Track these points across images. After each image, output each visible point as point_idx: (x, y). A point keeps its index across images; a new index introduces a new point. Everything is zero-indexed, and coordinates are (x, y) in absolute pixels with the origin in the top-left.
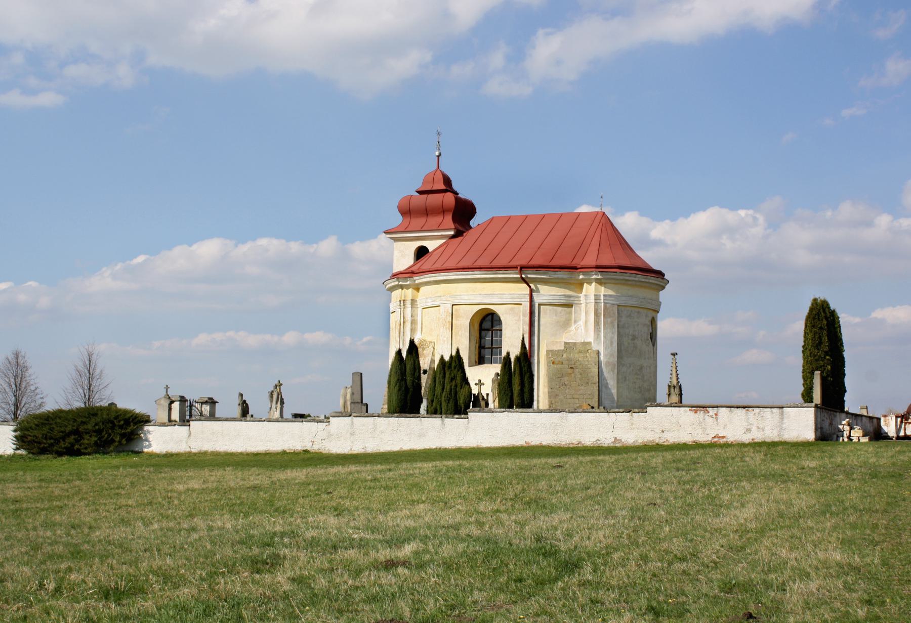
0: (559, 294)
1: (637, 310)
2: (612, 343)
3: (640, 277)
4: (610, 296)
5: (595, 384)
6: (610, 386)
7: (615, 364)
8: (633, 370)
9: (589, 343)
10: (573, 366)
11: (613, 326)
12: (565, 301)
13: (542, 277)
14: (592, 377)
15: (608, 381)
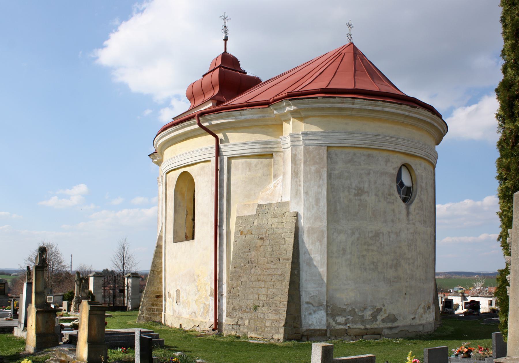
0: (253, 140)
1: (366, 152)
2: (317, 201)
3: (390, 107)
4: (314, 134)
5: (288, 260)
6: (315, 263)
7: (322, 231)
8: (358, 239)
9: (286, 204)
10: (263, 236)
11: (320, 177)
12: (259, 150)
13: (227, 121)
14: (285, 250)
15: (312, 256)
